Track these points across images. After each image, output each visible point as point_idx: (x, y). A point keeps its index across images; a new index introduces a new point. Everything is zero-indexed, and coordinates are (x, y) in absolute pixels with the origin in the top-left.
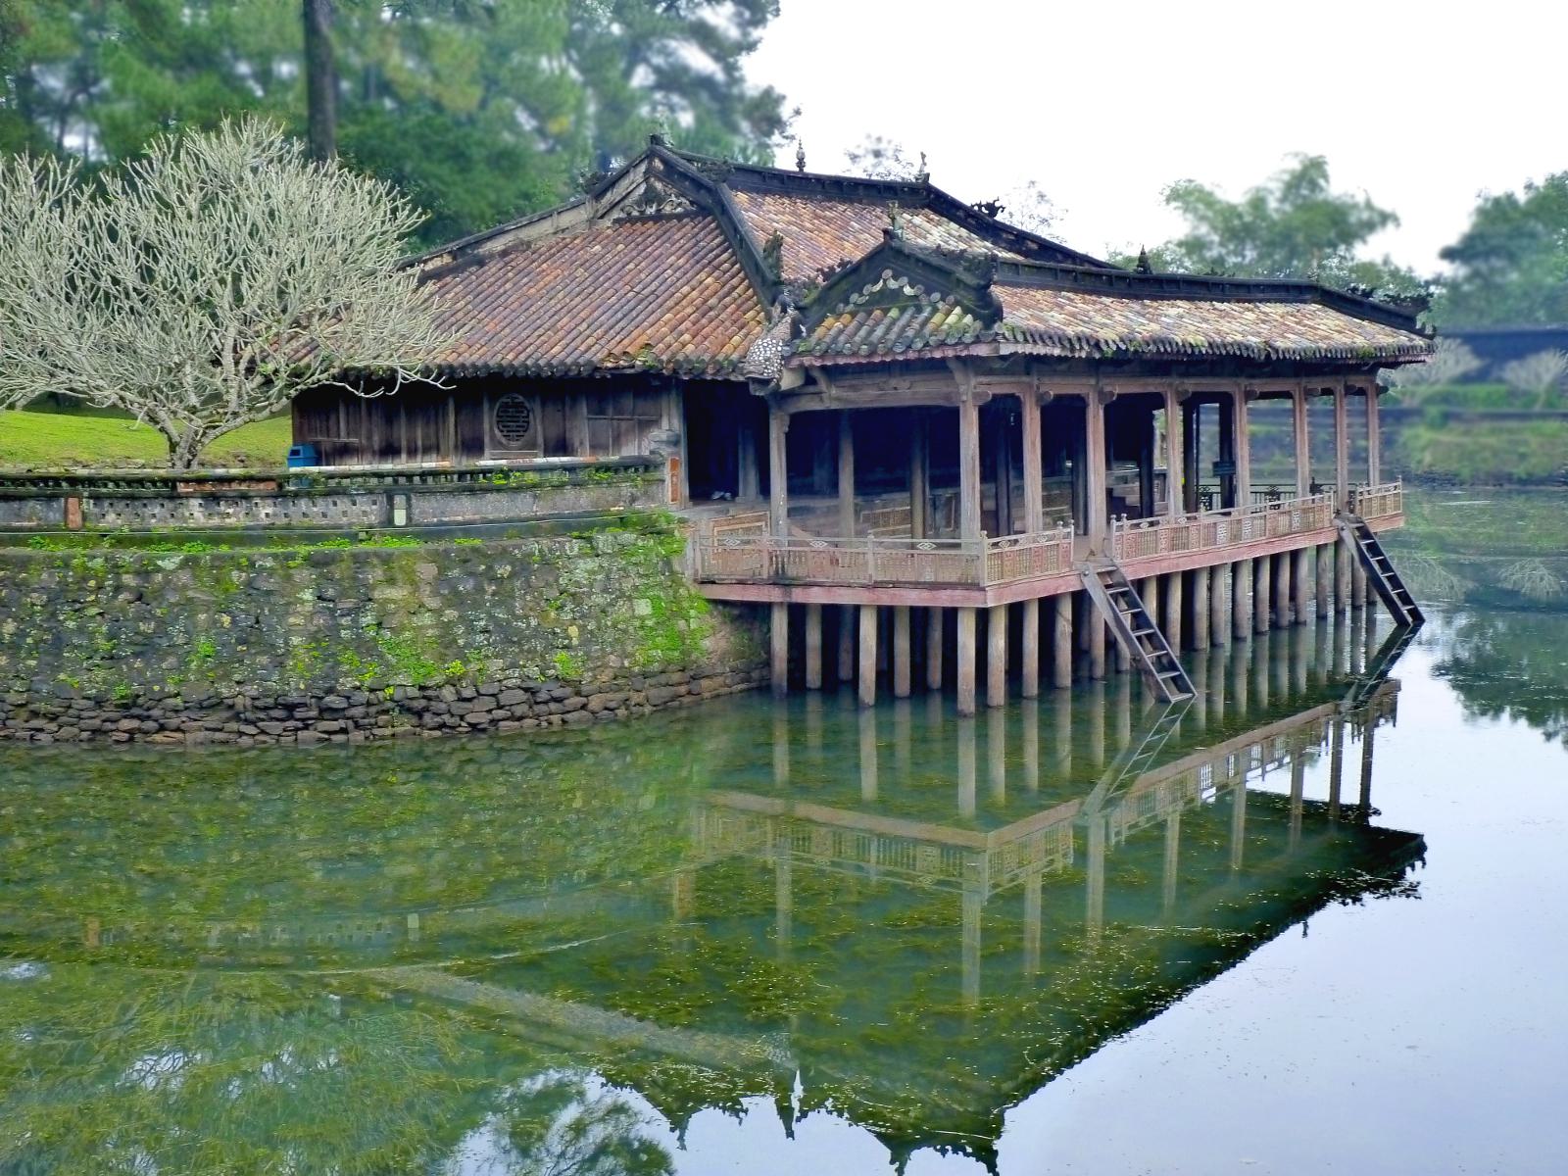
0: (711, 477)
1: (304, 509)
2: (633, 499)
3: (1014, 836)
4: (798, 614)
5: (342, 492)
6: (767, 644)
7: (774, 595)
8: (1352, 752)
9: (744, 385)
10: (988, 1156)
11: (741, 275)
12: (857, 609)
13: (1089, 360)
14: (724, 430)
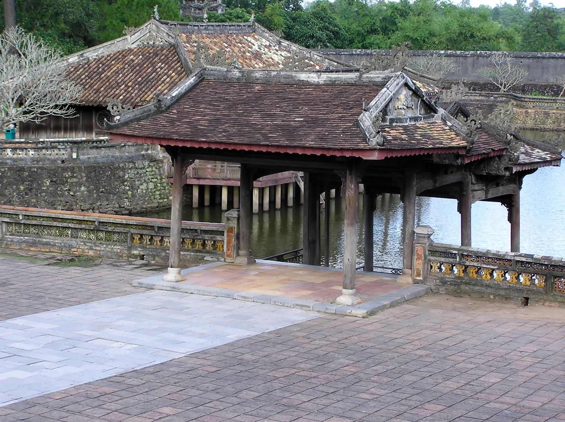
2: (147, 150)
4: (202, 188)
5: (56, 147)
6: (192, 198)
11: (184, 73)
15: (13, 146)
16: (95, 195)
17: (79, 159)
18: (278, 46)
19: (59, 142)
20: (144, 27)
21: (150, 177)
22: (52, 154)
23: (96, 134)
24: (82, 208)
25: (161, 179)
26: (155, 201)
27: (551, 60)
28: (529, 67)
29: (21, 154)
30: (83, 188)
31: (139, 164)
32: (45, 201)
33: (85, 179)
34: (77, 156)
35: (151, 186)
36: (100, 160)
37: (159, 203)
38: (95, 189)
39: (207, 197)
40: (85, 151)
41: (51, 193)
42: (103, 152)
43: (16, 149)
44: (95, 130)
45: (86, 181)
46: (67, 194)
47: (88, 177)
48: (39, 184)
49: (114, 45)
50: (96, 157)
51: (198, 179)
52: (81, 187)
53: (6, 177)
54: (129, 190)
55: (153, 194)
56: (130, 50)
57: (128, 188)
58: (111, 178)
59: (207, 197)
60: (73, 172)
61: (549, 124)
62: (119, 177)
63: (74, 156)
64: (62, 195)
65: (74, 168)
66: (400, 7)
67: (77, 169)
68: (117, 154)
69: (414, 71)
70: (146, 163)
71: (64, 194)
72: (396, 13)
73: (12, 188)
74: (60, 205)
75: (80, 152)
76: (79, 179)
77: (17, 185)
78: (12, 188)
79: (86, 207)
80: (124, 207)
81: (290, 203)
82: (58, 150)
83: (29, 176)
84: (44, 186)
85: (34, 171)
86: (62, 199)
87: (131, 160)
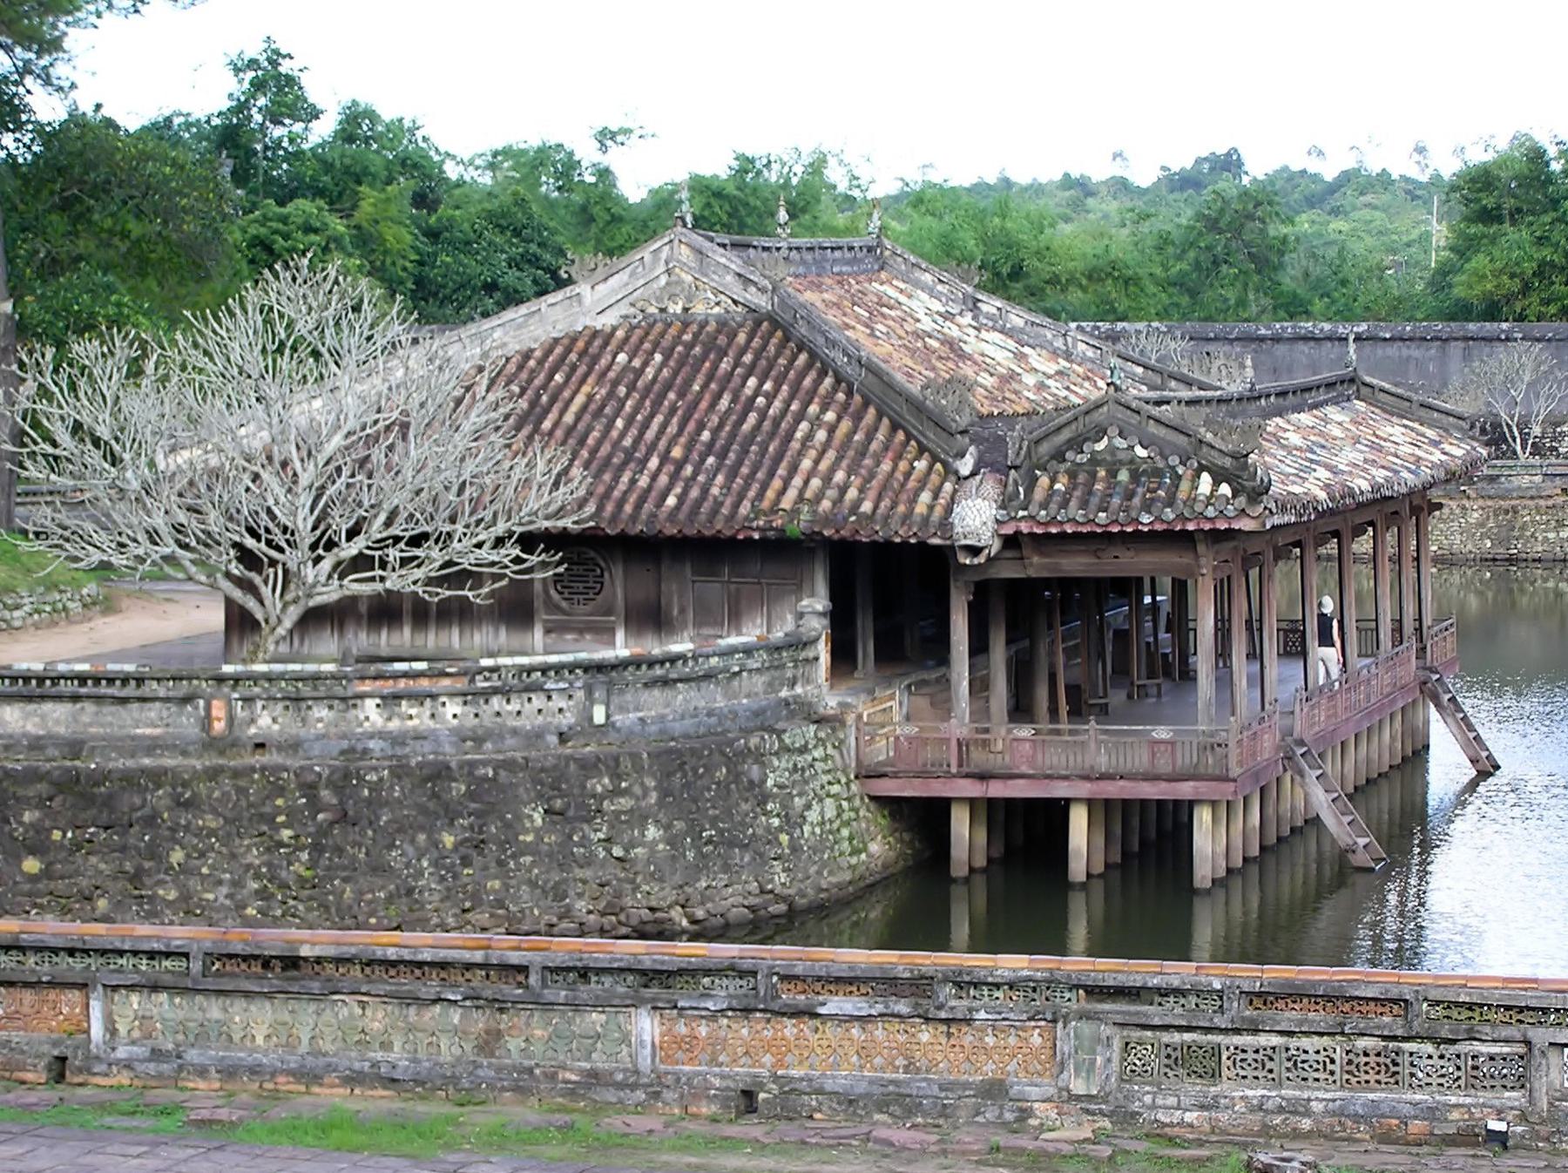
1: (497, 708)
11: (872, 411)
12: (1191, 804)
13: (1152, 534)
14: (891, 598)
15: (388, 687)
16: (690, 855)
17: (613, 724)
18: (970, 315)
19: (545, 669)
20: (646, 253)
21: (826, 778)
22: (525, 712)
23: (548, 631)
24: (654, 904)
27: (1303, 347)
29: (417, 717)
30: (652, 832)
32: (533, 884)
33: (653, 797)
34: (608, 717)
36: (678, 728)
37: (852, 868)
38: (687, 834)
40: (628, 697)
41: (550, 855)
42: (683, 697)
43: (397, 697)
44: (542, 616)
45: (661, 803)
46: (602, 854)
47: (665, 793)
48: (508, 825)
49: (537, 317)
50: (662, 718)
51: (983, 777)
52: (643, 829)
53: (387, 803)
54: (780, 829)
57: (776, 822)
58: (729, 791)
60: (617, 776)
64: (589, 861)
65: (616, 760)
66: (731, 189)
67: (626, 764)
69: (1400, 391)
71: (593, 855)
72: (717, 209)
73: (413, 841)
74: (580, 896)
75: (615, 700)
76: (638, 799)
77: (431, 831)
78: (413, 841)
79: (664, 899)
80: (771, 892)
82: (543, 697)
83: (471, 795)
84: (527, 832)
85: (485, 779)
86: (587, 873)
87: (763, 721)
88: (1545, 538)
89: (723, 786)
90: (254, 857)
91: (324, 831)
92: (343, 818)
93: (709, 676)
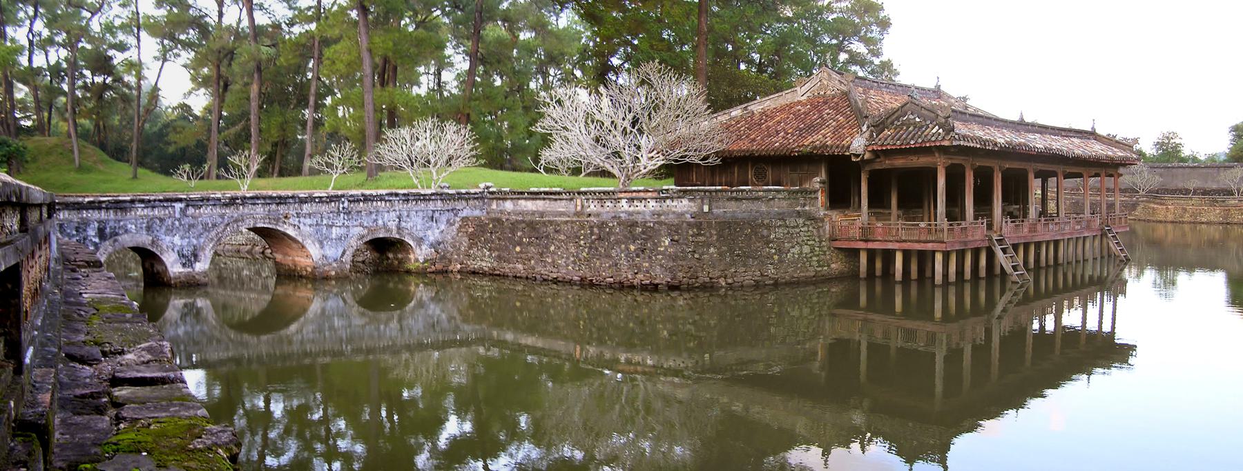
0: (840, 197)
2: (804, 205)
3: (939, 335)
7: (861, 245)
8: (1108, 307)
9: (849, 157)
10: (943, 462)
12: (934, 252)
13: (992, 151)
14: (842, 176)
25: (820, 242)
26: (811, 269)
28: (1161, 175)
29: (640, 207)
31: (791, 222)
32: (661, 266)
35: (806, 249)
36: (740, 216)
39: (879, 265)
42: (745, 205)
47: (720, 236)
51: (866, 241)
55: (809, 259)
56: (799, 102)
59: (879, 265)
61: (1187, 218)
62: (763, 236)
63: (706, 209)
68: (764, 208)
70: (801, 221)
75: (714, 204)
81: (983, 273)
83: (643, 233)
87: (782, 217)
88: (1238, 218)
89: (749, 237)
90: (573, 250)
91: (593, 242)
92: (599, 238)
93: (757, 199)
